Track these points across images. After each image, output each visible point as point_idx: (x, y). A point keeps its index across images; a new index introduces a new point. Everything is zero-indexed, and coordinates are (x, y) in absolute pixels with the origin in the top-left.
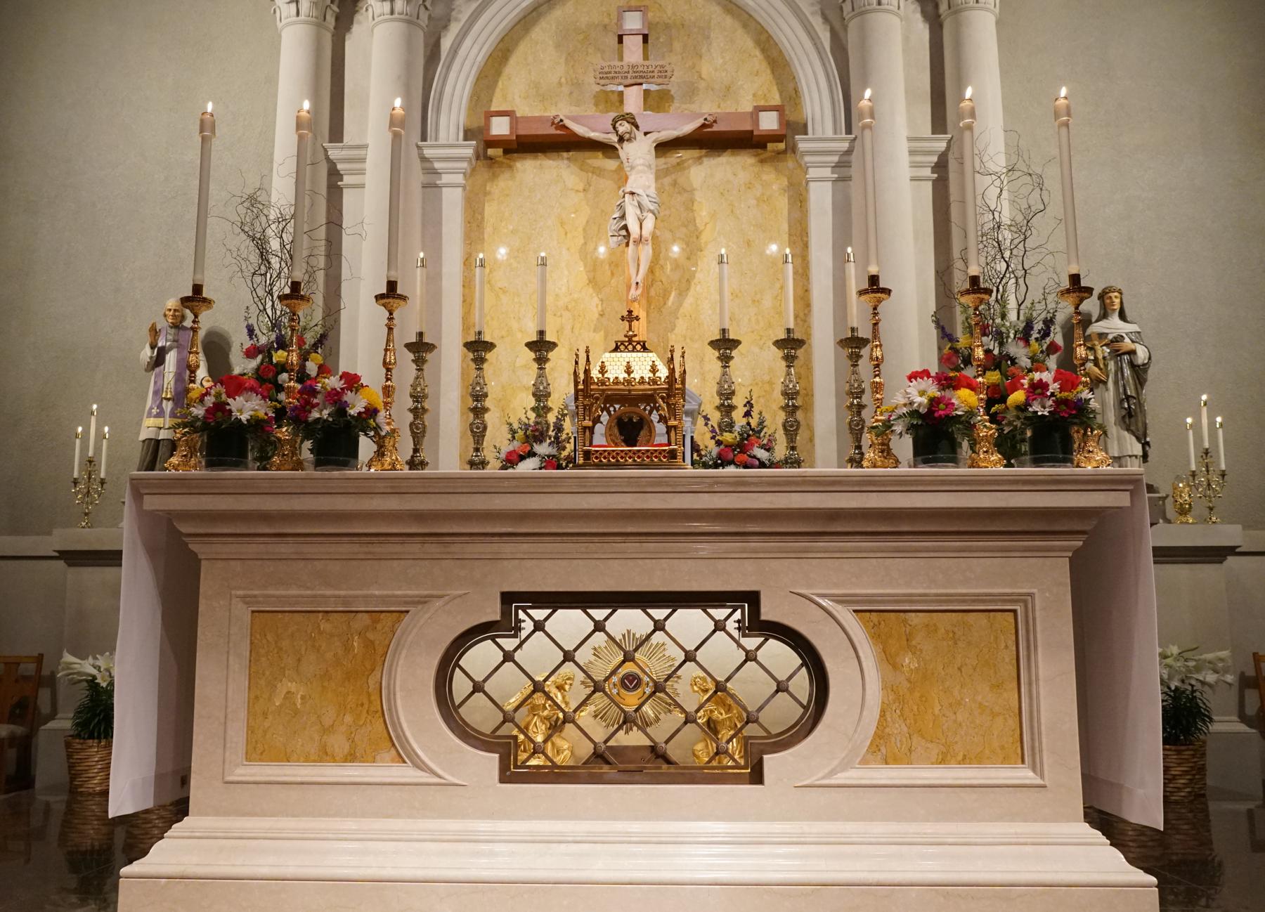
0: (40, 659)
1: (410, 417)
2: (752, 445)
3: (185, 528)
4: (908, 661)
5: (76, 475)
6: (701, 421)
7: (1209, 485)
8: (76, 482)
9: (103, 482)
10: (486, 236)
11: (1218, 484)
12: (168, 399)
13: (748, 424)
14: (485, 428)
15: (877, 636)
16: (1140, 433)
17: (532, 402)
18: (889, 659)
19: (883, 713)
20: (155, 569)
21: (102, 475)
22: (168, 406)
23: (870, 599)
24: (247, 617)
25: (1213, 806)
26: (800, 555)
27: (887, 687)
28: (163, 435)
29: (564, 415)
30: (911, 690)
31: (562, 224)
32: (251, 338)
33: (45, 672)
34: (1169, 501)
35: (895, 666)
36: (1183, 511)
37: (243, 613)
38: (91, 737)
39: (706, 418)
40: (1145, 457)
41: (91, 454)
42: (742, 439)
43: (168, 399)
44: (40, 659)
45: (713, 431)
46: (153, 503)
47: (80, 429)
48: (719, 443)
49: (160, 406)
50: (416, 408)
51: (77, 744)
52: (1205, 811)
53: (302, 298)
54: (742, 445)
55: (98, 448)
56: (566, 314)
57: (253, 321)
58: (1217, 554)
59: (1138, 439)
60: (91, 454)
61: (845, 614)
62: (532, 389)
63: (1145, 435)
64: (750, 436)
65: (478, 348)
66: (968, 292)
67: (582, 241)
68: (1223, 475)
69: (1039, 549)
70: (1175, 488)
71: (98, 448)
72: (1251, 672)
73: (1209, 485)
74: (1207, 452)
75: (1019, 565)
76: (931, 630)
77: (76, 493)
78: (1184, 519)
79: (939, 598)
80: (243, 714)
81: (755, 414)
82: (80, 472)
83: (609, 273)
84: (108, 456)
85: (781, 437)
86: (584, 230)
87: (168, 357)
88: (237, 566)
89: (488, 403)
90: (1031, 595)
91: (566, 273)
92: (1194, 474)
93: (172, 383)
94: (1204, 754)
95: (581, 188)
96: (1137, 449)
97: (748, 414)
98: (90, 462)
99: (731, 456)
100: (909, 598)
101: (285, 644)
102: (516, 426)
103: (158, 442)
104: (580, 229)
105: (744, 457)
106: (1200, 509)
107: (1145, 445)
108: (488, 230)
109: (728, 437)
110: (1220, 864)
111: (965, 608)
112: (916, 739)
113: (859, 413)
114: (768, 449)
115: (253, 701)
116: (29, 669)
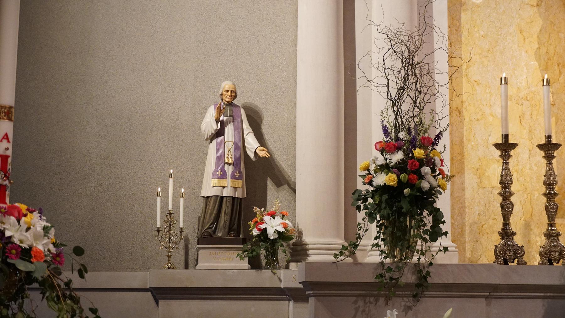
1: (544, 200)
5: (159, 225)
10: (463, 39)
12: (230, 164)
21: (181, 225)
22: (229, 170)
28: (227, 193)
31: (521, 32)
32: (387, 137)
41: (170, 207)
43: (230, 164)
49: (223, 170)
50: (550, 193)
56: (526, 103)
57: (385, 123)
60: (170, 207)
62: (543, 179)
65: (506, 147)
67: (537, 46)
82: (161, 223)
83: (558, 72)
86: (538, 37)
87: (226, 129)
89: (513, 188)
91: (525, 71)
93: (232, 150)
95: (535, 4)
98: (170, 214)
103: (222, 198)
104: (535, 36)
108: (465, 34)
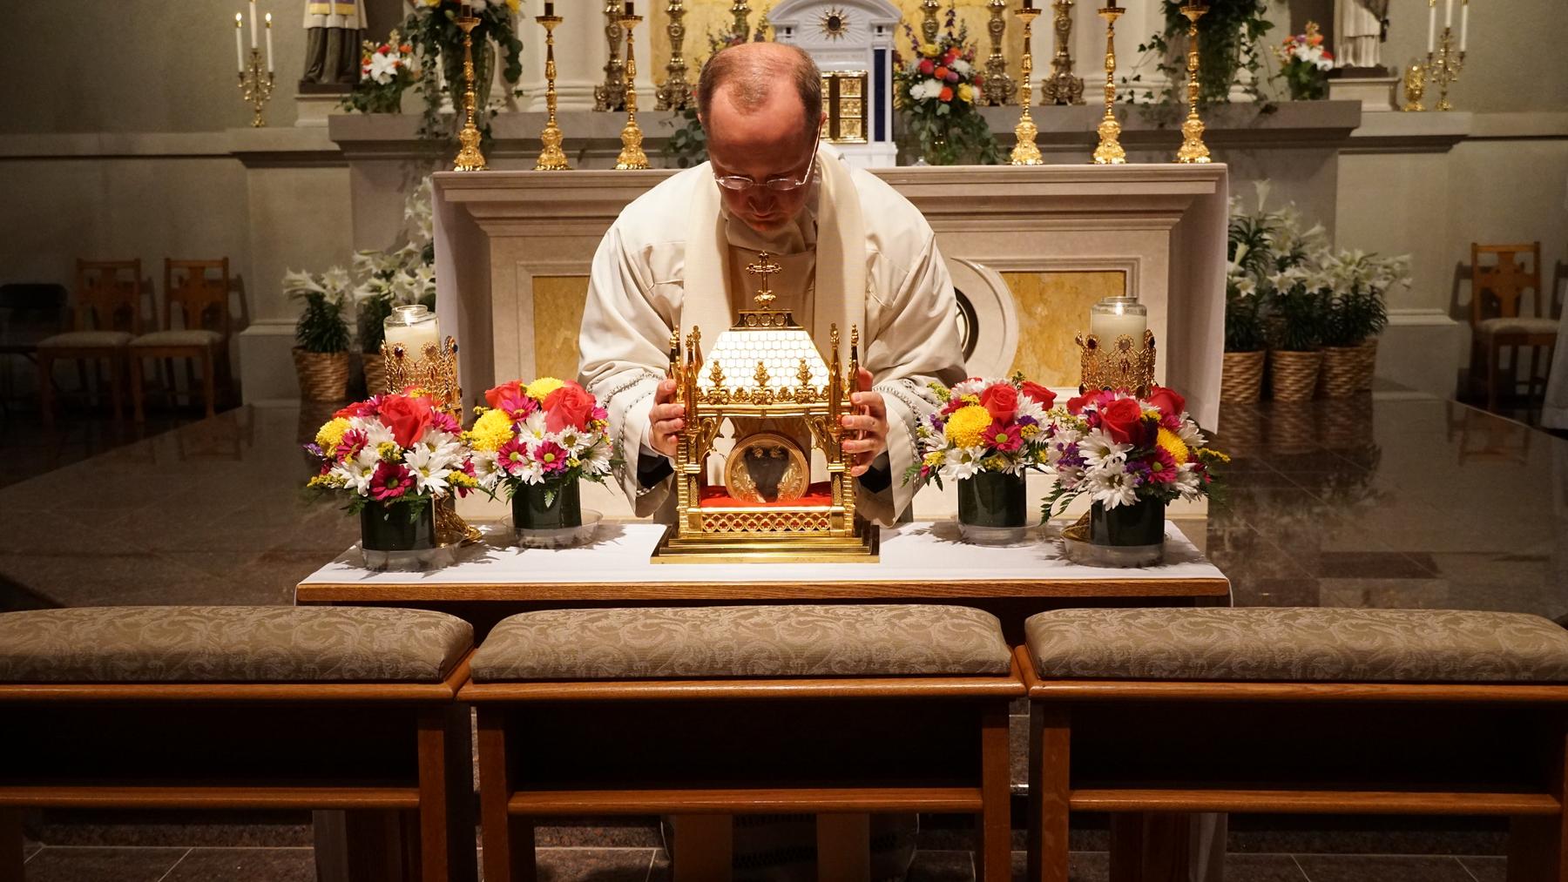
0: (225, 263)
2: (953, 57)
3: (476, 214)
4: (1040, 310)
6: (903, 31)
7: (1445, 68)
8: (242, 76)
9: (271, 76)
11: (1455, 67)
13: (950, 34)
14: (683, 31)
15: (1017, 291)
16: (1380, 10)
17: (732, 19)
18: (1026, 309)
19: (1019, 350)
20: (449, 238)
23: (1013, 263)
24: (530, 281)
25: (1376, 396)
26: (959, 230)
27: (1023, 329)
29: (765, 27)
30: (1041, 333)
33: (232, 275)
34: (1401, 86)
35: (1030, 314)
36: (1413, 98)
37: (526, 278)
38: (325, 350)
39: (908, 28)
40: (1383, 36)
42: (944, 52)
44: (225, 263)
45: (915, 42)
46: (452, 196)
47: (239, 17)
48: (920, 55)
51: (311, 357)
52: (1369, 405)
53: (555, 19)
54: (942, 59)
55: (261, 38)
58: (1442, 143)
59: (1377, 17)
60: (254, 45)
61: (993, 276)
63: (1385, 11)
64: (952, 46)
66: (1105, 11)
68: (1462, 56)
69: (1149, 224)
70: (1409, 70)
71: (261, 38)
72: (1468, 262)
73: (1445, 68)
74: (1447, 31)
75: (1130, 236)
76: (1059, 286)
77: (244, 89)
78: (1412, 106)
79: (1067, 262)
80: (532, 355)
81: (957, 23)
84: (273, 41)
85: (986, 40)
88: (520, 242)
90: (1137, 260)
92: (1430, 56)
94: (1374, 353)
96: (1374, 27)
97: (950, 23)
99: (931, 69)
100: (1043, 263)
101: (561, 301)
102: (717, 37)
103: (325, 30)
105: (944, 71)
106: (1432, 92)
107: (1385, 23)
109: (929, 49)
110: (1379, 452)
111: (1085, 270)
112: (1044, 368)
113: (1067, 13)
114: (968, 59)
115: (539, 345)
116: (215, 273)
